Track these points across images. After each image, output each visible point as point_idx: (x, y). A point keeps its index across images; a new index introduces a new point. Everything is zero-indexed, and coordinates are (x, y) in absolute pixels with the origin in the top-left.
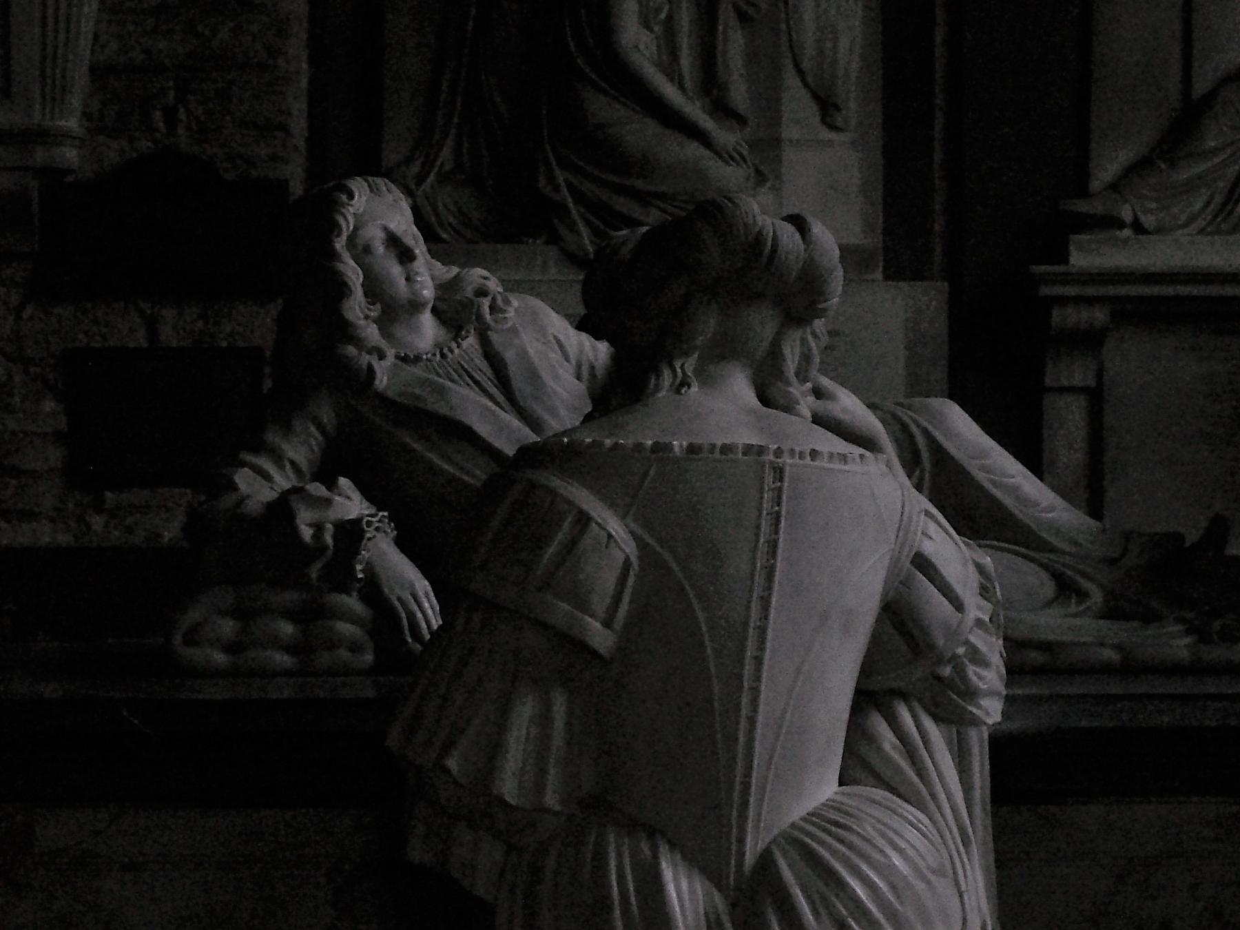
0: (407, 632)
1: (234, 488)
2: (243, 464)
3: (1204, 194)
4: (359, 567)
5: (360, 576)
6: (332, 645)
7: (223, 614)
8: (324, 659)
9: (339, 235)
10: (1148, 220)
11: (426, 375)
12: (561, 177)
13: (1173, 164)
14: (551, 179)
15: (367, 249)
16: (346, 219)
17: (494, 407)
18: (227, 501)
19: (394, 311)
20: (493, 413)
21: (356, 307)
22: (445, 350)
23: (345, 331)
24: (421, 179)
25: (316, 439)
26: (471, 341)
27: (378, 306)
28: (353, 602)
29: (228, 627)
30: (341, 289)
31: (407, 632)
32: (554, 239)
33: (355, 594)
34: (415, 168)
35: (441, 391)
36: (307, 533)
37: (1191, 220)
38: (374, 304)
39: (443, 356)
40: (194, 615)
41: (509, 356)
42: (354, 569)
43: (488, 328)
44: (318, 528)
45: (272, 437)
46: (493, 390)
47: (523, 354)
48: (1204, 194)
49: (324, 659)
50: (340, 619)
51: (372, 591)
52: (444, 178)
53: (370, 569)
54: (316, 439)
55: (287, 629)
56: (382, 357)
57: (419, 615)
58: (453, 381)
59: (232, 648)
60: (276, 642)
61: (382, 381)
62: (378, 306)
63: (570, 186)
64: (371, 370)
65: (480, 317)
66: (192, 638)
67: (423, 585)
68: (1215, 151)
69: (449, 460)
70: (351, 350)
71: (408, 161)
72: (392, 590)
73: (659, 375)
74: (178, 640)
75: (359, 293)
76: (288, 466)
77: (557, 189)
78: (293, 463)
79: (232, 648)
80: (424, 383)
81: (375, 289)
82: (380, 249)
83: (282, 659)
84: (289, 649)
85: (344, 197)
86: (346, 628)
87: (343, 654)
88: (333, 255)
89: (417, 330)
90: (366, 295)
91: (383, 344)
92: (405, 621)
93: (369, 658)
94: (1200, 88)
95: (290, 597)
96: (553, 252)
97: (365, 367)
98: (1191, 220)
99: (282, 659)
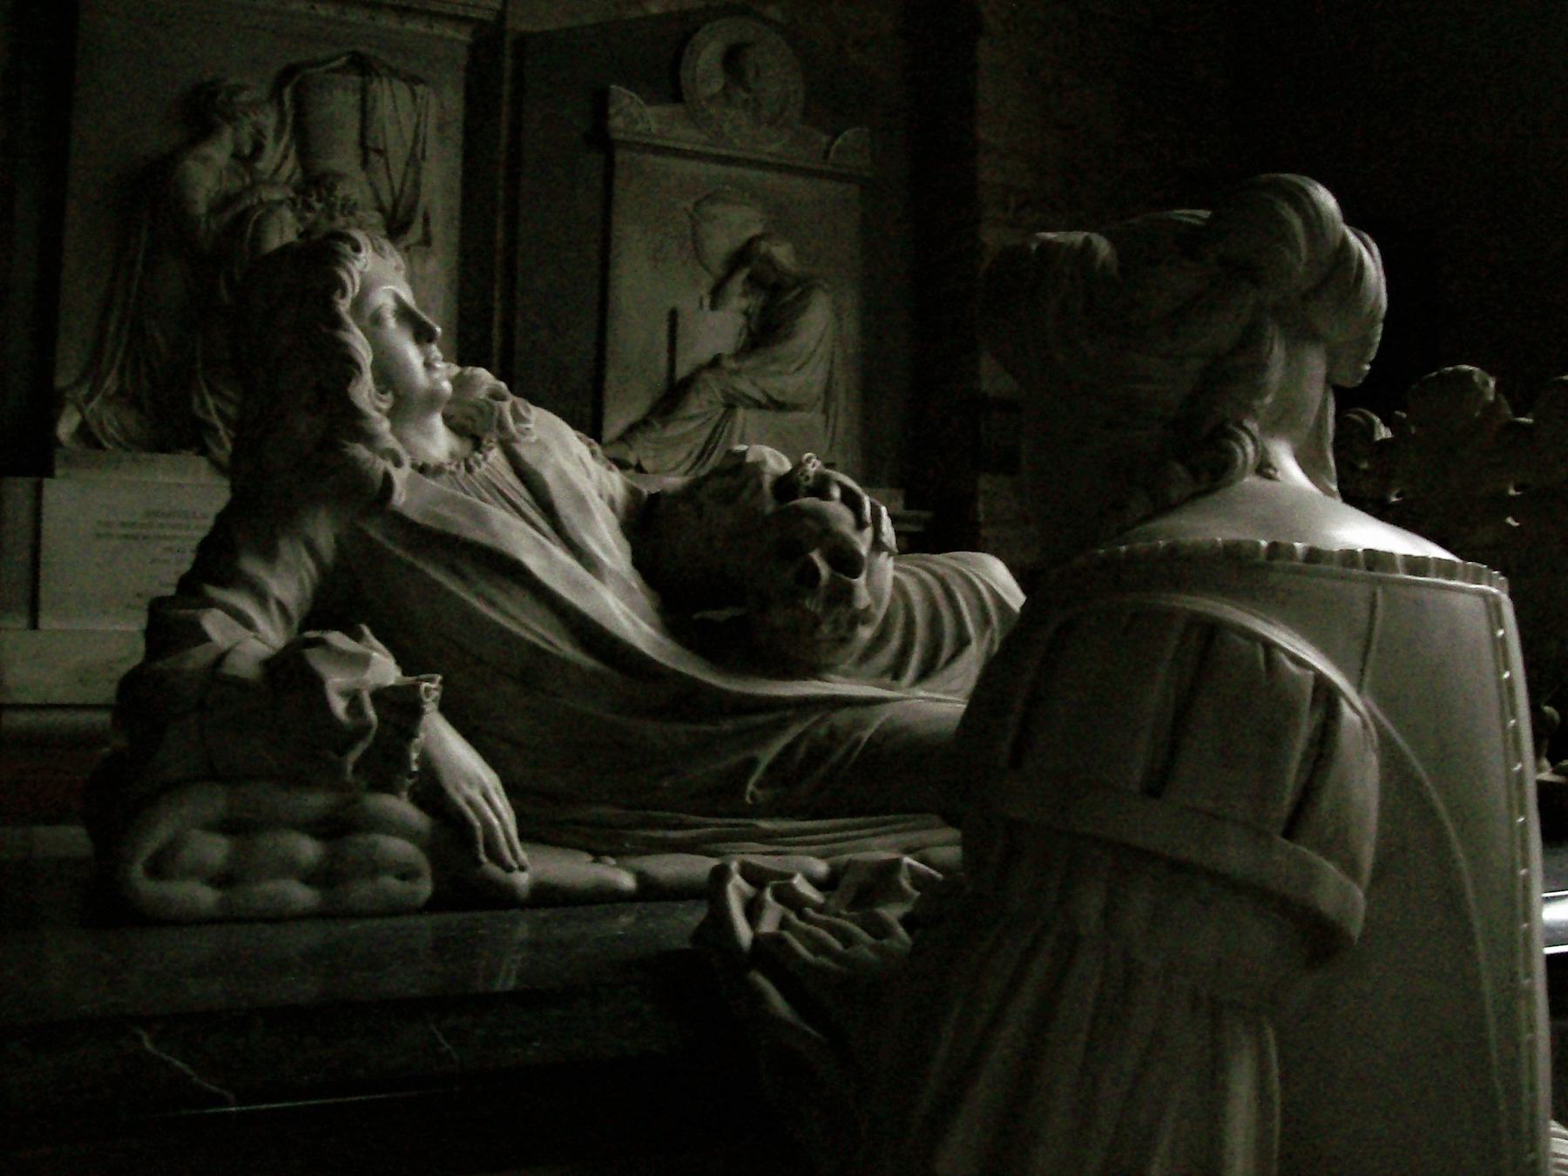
0: (481, 847)
1: (204, 638)
2: (211, 603)
3: (686, 448)
4: (414, 756)
5: (415, 768)
6: (375, 867)
7: (209, 827)
8: (361, 892)
9: (344, 295)
10: (647, 464)
11: (451, 491)
12: (210, 402)
13: (664, 425)
14: (203, 403)
15: (377, 319)
16: (352, 277)
17: (541, 538)
18: (199, 657)
19: (406, 404)
20: (539, 542)
21: (364, 392)
22: (472, 462)
23: (353, 423)
24: (89, 398)
25: (308, 571)
26: (495, 455)
27: (389, 396)
28: (400, 806)
29: (215, 849)
30: (349, 366)
31: (481, 847)
32: (204, 451)
33: (405, 794)
34: (85, 391)
35: (478, 516)
36: (339, 706)
37: (678, 466)
38: (383, 393)
39: (469, 469)
40: (162, 833)
41: (549, 476)
42: (408, 757)
43: (514, 439)
44: (354, 699)
45: (252, 565)
46: (534, 516)
47: (562, 475)
48: (686, 448)
49: (361, 892)
50: (388, 833)
51: (432, 792)
52: (108, 400)
53: (427, 762)
54: (308, 571)
55: (308, 849)
56: (398, 463)
57: (496, 822)
58: (485, 501)
59: (223, 880)
60: (289, 868)
61: (400, 498)
62: (389, 396)
63: (219, 411)
64: (387, 478)
65: (502, 426)
66: (158, 868)
67: (490, 778)
68: (691, 418)
69: (492, 604)
70: (361, 451)
71: (78, 383)
72: (458, 789)
73: (1238, 440)
74: (137, 870)
75: (368, 376)
76: (273, 607)
77: (208, 412)
78: (281, 606)
79: (223, 880)
80: (451, 501)
81: (388, 375)
82: (391, 323)
83: (302, 896)
84: (310, 878)
85: (348, 248)
86: (398, 847)
87: (390, 882)
88: (337, 322)
89: (429, 434)
90: (377, 381)
91: (398, 447)
92: (480, 834)
93: (425, 888)
94: (682, 371)
95: (316, 801)
96: (203, 463)
97: (380, 473)
98: (678, 466)
99: (302, 896)
